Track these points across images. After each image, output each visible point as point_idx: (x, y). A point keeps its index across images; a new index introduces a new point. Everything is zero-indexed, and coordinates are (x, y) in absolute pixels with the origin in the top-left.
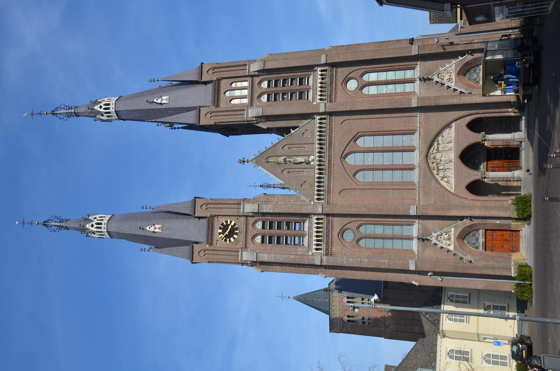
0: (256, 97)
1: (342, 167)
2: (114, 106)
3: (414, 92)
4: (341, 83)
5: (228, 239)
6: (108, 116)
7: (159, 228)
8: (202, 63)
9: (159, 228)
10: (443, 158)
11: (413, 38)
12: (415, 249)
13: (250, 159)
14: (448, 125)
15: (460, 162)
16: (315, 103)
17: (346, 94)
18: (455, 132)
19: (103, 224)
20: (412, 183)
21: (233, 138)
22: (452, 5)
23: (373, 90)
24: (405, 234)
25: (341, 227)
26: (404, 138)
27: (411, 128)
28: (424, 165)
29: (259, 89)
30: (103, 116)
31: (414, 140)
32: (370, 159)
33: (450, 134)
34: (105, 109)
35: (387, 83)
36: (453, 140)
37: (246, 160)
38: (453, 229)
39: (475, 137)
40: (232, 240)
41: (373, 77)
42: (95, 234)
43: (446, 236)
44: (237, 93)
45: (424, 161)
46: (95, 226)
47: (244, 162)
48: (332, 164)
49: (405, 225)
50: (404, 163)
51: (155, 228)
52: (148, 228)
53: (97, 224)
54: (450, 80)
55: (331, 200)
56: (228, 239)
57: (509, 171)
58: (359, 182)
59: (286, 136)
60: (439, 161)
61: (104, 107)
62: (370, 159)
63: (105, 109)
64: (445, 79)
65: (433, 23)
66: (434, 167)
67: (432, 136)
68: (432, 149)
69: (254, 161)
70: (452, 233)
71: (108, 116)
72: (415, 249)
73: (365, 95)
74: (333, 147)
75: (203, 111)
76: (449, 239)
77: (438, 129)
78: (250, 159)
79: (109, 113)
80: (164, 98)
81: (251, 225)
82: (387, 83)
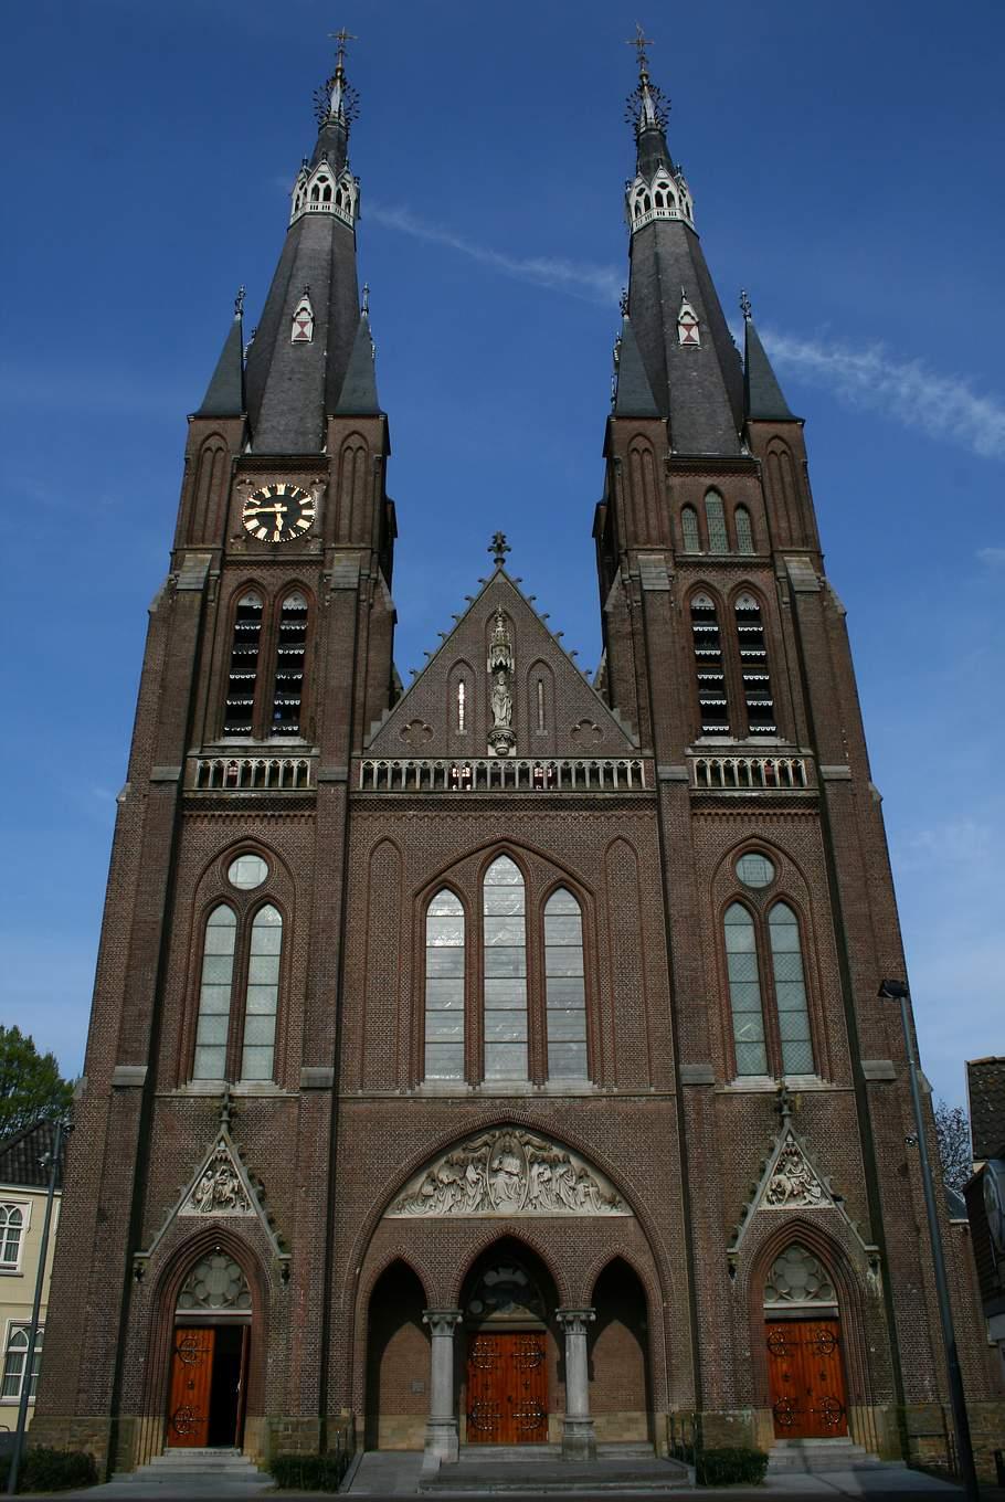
1: (476, 845)
2: (667, 216)
3: (736, 1074)
4: (758, 832)
6: (637, 208)
8: (803, 421)
10: (501, 1178)
11: (906, 994)
13: (506, 567)
14: (620, 1192)
15: (487, 1236)
16: (689, 751)
17: (721, 850)
18: (596, 1219)
19: (327, 203)
21: (590, 545)
23: (740, 938)
25: (274, 844)
26: (574, 1046)
27: (609, 1067)
28: (479, 1114)
29: (731, 585)
30: (639, 194)
31: (570, 1081)
32: (506, 932)
33: (587, 1203)
35: (767, 982)
36: (566, 1212)
37: (505, 555)
38: (252, 1213)
39: (577, 1281)
41: (785, 937)
42: (301, 189)
43: (227, 1190)
44: (716, 527)
45: (495, 1115)
46: (322, 186)
47: (500, 549)
50: (487, 1046)
51: (303, 325)
52: (305, 304)
54: (779, 1191)
55: (366, 814)
59: (598, 694)
60: (496, 1164)
62: (506, 932)
64: (781, 1177)
65: (970, 1074)
66: (475, 1150)
67: (580, 1138)
68: (536, 1141)
69: (500, 579)
70: (238, 1212)
71: (637, 208)
75: (656, 429)
76: (218, 1201)
77: (606, 1159)
78: (506, 567)
79: (648, 206)
80: (695, 333)
81: (294, 576)
82: (767, 982)
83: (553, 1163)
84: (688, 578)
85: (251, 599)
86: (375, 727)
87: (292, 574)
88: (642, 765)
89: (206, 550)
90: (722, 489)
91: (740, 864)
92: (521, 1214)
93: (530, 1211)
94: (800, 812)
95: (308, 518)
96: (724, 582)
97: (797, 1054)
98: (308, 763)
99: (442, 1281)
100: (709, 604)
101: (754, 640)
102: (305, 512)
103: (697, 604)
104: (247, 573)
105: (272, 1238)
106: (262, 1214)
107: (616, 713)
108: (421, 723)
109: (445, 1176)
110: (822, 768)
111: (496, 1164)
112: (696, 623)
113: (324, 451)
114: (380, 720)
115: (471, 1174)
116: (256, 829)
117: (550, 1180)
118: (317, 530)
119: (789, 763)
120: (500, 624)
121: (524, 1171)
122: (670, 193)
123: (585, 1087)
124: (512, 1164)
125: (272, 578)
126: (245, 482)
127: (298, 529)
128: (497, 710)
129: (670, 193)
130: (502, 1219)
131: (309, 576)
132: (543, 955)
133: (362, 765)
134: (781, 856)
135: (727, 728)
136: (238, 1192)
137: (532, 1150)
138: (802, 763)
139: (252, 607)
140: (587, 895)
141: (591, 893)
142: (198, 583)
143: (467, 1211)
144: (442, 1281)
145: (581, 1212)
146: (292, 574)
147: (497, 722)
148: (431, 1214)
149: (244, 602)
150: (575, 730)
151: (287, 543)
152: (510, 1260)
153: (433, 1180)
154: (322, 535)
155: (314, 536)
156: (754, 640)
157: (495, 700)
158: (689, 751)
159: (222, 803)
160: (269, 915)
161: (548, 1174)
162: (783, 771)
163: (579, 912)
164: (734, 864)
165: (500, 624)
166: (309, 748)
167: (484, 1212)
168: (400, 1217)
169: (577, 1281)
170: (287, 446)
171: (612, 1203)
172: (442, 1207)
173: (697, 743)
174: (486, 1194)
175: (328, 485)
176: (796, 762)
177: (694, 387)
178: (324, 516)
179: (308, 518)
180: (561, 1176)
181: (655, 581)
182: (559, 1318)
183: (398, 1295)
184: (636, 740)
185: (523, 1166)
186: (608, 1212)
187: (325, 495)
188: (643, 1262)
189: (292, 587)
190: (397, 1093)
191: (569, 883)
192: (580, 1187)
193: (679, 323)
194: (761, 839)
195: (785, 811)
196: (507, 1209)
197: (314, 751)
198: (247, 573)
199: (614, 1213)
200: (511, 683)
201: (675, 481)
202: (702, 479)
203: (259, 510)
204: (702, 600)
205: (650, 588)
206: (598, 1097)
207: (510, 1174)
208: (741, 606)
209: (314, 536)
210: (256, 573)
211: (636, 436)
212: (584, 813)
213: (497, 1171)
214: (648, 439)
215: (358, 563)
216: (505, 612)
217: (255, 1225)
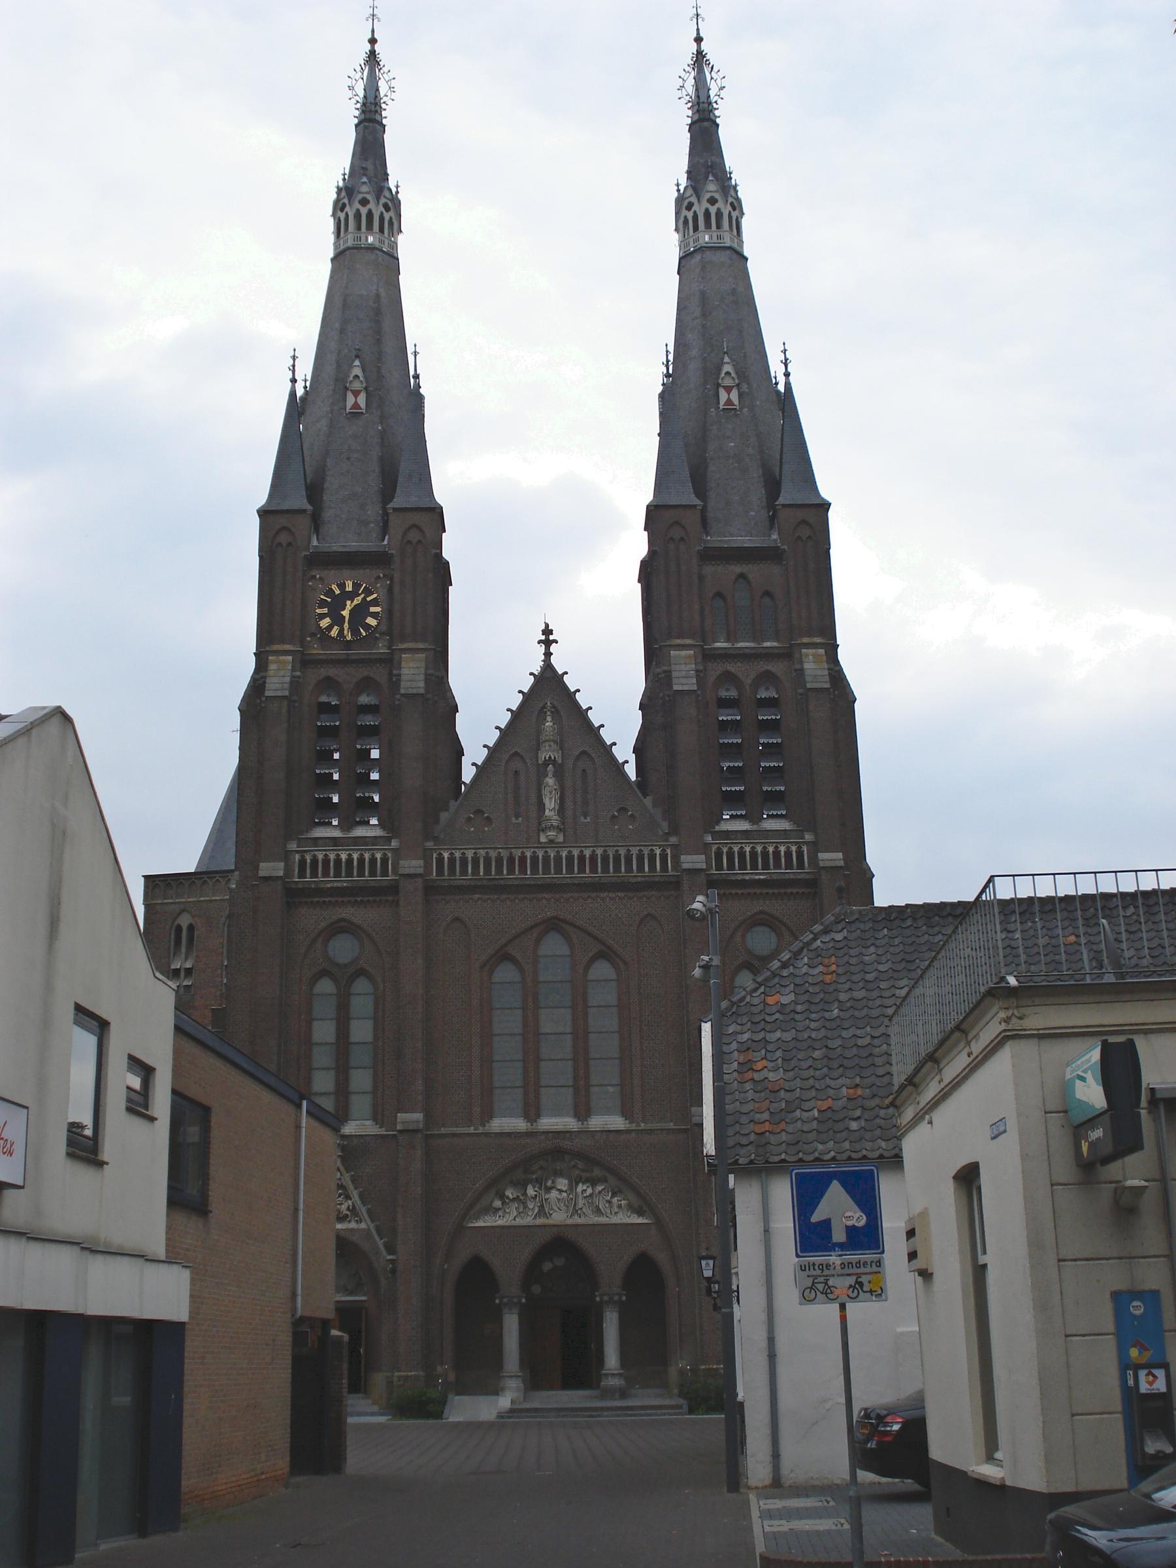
0: (769, 667)
5: (325, 610)
7: (356, 405)
9: (356, 405)
10: (554, 1194)
12: (498, 1124)
16: (709, 839)
20: (488, 1114)
22: (807, 1196)
24: (546, 1096)
26: (611, 1089)
29: (753, 675)
34: (707, 214)
36: (602, 1220)
38: (363, 1226)
39: (611, 1271)
40: (372, 621)
46: (364, 211)
48: (540, 896)
49: (526, 1094)
50: (543, 1090)
51: (356, 394)
53: (370, 215)
56: (325, 610)
57: (523, 1363)
58: (491, 972)
60: (549, 1183)
61: (713, 210)
63: (707, 214)
70: (353, 1225)
72: (498, 1124)
73: (732, 980)
74: (585, 895)
81: (366, 674)
83: (593, 1182)
84: (716, 669)
85: (328, 695)
86: (444, 816)
87: (364, 672)
88: (669, 851)
89: (286, 653)
90: (750, 576)
91: (749, 936)
92: (570, 1222)
93: (577, 1220)
94: (801, 891)
95: (375, 615)
96: (747, 673)
97: (606, 1077)
98: (390, 855)
99: (509, 1271)
100: (733, 693)
101: (771, 727)
102: (372, 609)
103: (723, 694)
104: (324, 672)
105: (380, 1243)
106: (372, 1226)
107: (648, 801)
108: (482, 812)
109: (510, 1193)
110: (821, 856)
111: (549, 1183)
112: (721, 711)
113: (386, 542)
114: (447, 810)
115: (531, 1191)
116: (348, 913)
117: (591, 1195)
118: (384, 628)
119: (794, 848)
120: (549, 719)
121: (572, 1188)
122: (719, 209)
123: (617, 1122)
124: (562, 1183)
125: (347, 676)
126: (315, 577)
127: (367, 627)
128: (547, 801)
129: (719, 209)
130: (555, 1226)
131: (379, 674)
132: (586, 1014)
133: (435, 856)
134: (783, 929)
135: (744, 813)
136: (353, 1210)
137: (577, 1172)
138: (805, 848)
139: (329, 703)
140: (622, 966)
141: (625, 963)
142: (283, 689)
143: (528, 1220)
144: (509, 1271)
145: (616, 1220)
146: (364, 672)
147: (547, 812)
148: (500, 1222)
149: (323, 699)
150: (614, 816)
151: (358, 641)
152: (562, 1249)
153: (502, 1197)
154: (390, 633)
155: (382, 634)
156: (771, 727)
157: (546, 792)
158: (709, 839)
159: (319, 891)
160: (361, 986)
161: (589, 1191)
162: (788, 854)
163: (614, 977)
164: (743, 936)
165: (549, 719)
166: (388, 840)
167: (541, 1221)
168: (477, 1225)
169: (611, 1271)
170: (353, 544)
171: (640, 1213)
172: (508, 1218)
173: (717, 828)
174: (542, 1206)
175: (392, 580)
176: (800, 847)
177: (731, 461)
178: (389, 612)
179: (375, 615)
180: (600, 1192)
181: (684, 681)
182: (598, 1299)
183: (477, 1279)
184: (665, 826)
185: (570, 1185)
186: (636, 1220)
187: (390, 590)
188: (662, 1258)
189: (367, 684)
190: (472, 1130)
191: (605, 954)
192: (615, 1200)
193: (718, 385)
194: (767, 914)
195: (789, 891)
196: (559, 1217)
197: (394, 844)
198: (324, 672)
199: (640, 1220)
200: (559, 775)
201: (708, 570)
202: (732, 568)
203: (346, 625)
204: (728, 690)
205: (680, 688)
206: (628, 1131)
207: (560, 1191)
208: (763, 694)
209: (382, 634)
210: (332, 672)
211: (672, 525)
212: (620, 894)
213: (551, 1188)
214: (683, 527)
215: (423, 665)
216: (554, 707)
217: (367, 1233)
